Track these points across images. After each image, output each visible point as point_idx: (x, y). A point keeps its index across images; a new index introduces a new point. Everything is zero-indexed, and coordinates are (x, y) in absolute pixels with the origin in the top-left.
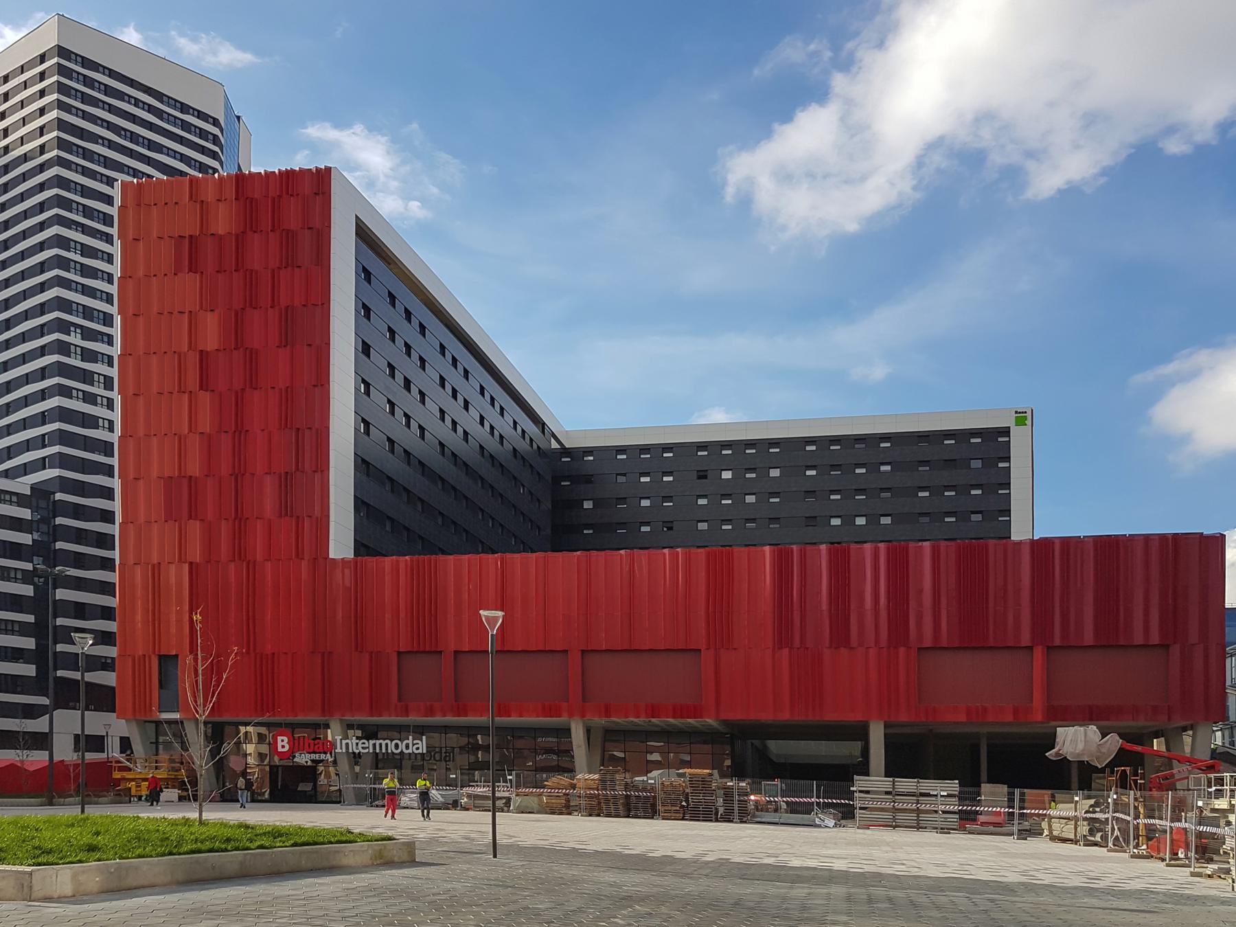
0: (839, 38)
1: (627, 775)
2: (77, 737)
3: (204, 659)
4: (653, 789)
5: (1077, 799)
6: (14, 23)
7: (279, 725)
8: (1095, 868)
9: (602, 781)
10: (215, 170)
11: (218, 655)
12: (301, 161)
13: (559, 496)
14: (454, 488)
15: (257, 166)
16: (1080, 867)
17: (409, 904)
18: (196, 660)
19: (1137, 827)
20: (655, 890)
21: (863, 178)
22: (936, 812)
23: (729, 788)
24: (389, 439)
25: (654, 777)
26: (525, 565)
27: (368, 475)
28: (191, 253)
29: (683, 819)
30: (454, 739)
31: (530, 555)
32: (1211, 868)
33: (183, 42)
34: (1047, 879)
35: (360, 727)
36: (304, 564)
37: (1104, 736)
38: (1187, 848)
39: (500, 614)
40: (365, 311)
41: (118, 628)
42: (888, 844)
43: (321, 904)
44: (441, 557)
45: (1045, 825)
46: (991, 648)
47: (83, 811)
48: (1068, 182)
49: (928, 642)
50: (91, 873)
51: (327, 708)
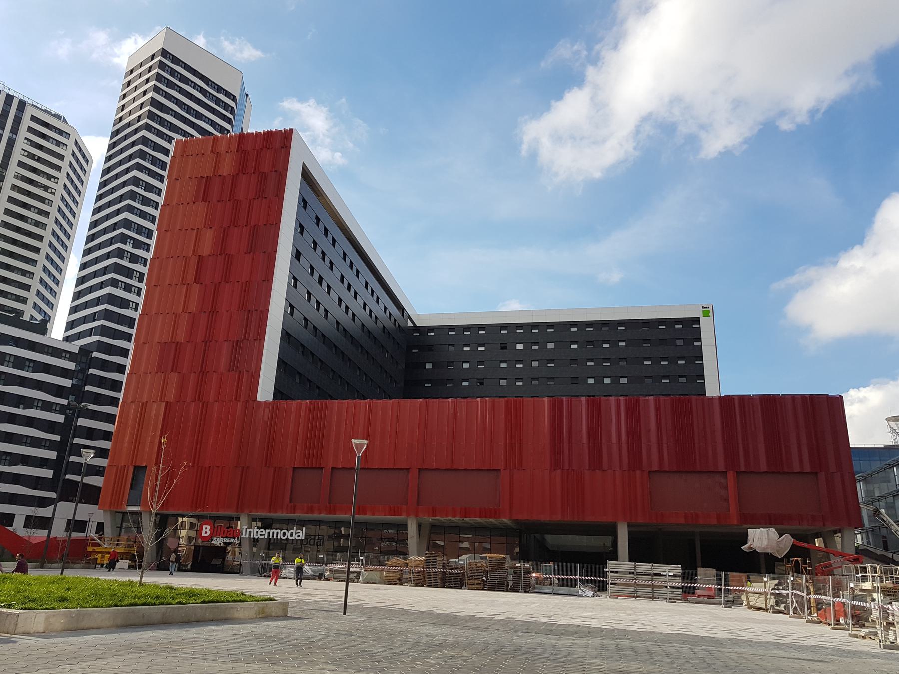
0: (592, 41)
1: (445, 558)
2: (69, 521)
3: (164, 469)
4: (462, 568)
5: (765, 579)
6: (144, 34)
7: (205, 517)
8: (781, 629)
9: (427, 561)
10: (228, 131)
11: (173, 467)
12: (277, 125)
13: (414, 360)
14: (342, 353)
15: (251, 130)
16: (770, 628)
17: (279, 646)
18: (158, 470)
19: (809, 601)
20: (460, 639)
21: (604, 141)
22: (666, 587)
23: (517, 567)
24: (305, 318)
25: (464, 559)
26: (384, 406)
27: (289, 343)
28: (205, 188)
29: (483, 589)
30: (325, 530)
31: (388, 401)
32: (863, 631)
33: (226, 45)
34: (747, 636)
35: (261, 520)
36: (240, 404)
37: (780, 536)
38: (846, 616)
39: (365, 442)
40: (301, 228)
41: (112, 446)
42: (631, 609)
43: (215, 644)
44: (330, 401)
45: (743, 597)
46: (699, 472)
47: (62, 573)
48: (725, 147)
49: (655, 467)
50: (59, 616)
51: (240, 507)
